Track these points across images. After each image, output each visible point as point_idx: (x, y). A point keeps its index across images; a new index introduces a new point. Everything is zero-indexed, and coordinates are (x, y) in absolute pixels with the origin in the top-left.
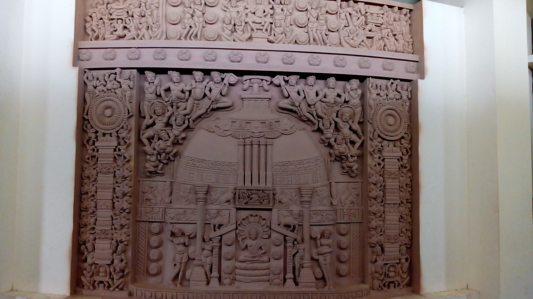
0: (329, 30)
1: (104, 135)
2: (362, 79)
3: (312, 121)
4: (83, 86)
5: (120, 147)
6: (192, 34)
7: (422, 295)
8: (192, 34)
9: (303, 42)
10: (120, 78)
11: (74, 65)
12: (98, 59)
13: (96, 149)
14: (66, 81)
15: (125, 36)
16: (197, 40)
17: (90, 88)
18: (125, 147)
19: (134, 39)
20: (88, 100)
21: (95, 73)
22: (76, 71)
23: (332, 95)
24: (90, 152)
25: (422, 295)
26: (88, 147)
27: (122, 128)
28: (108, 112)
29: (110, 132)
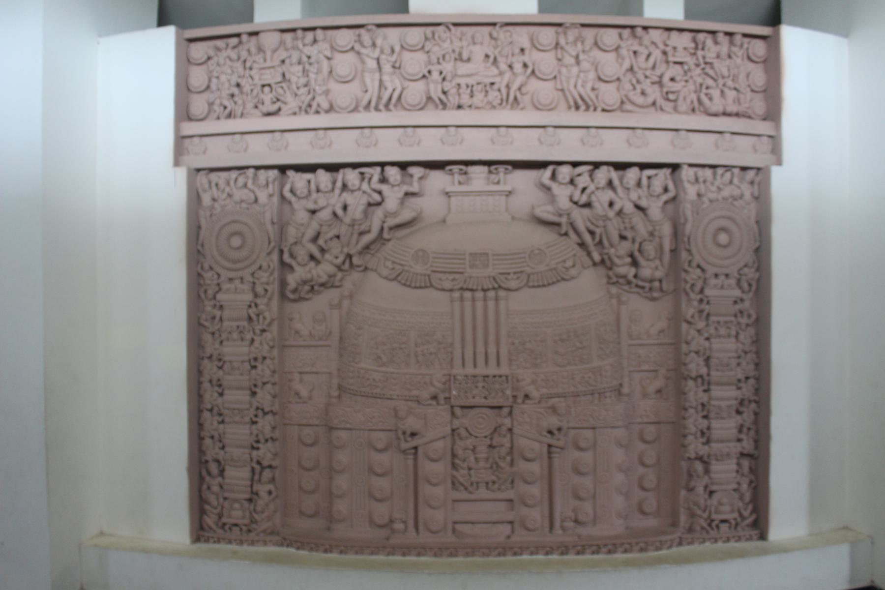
0: (600, 79)
1: (716, 276)
2: (675, 167)
3: (594, 247)
4: (194, 198)
5: (258, 301)
6: (390, 99)
7: (872, 581)
8: (390, 99)
9: (414, 106)
10: (253, 183)
11: (177, 163)
12: (218, 153)
13: (705, 300)
14: (164, 189)
15: (279, 110)
16: (369, 111)
17: (206, 199)
18: (265, 300)
19: (295, 114)
20: (203, 222)
21: (214, 176)
22: (182, 174)
23: (357, 202)
24: (208, 309)
25: (872, 581)
26: (206, 303)
27: (260, 268)
28: (236, 241)
29: (240, 274)
